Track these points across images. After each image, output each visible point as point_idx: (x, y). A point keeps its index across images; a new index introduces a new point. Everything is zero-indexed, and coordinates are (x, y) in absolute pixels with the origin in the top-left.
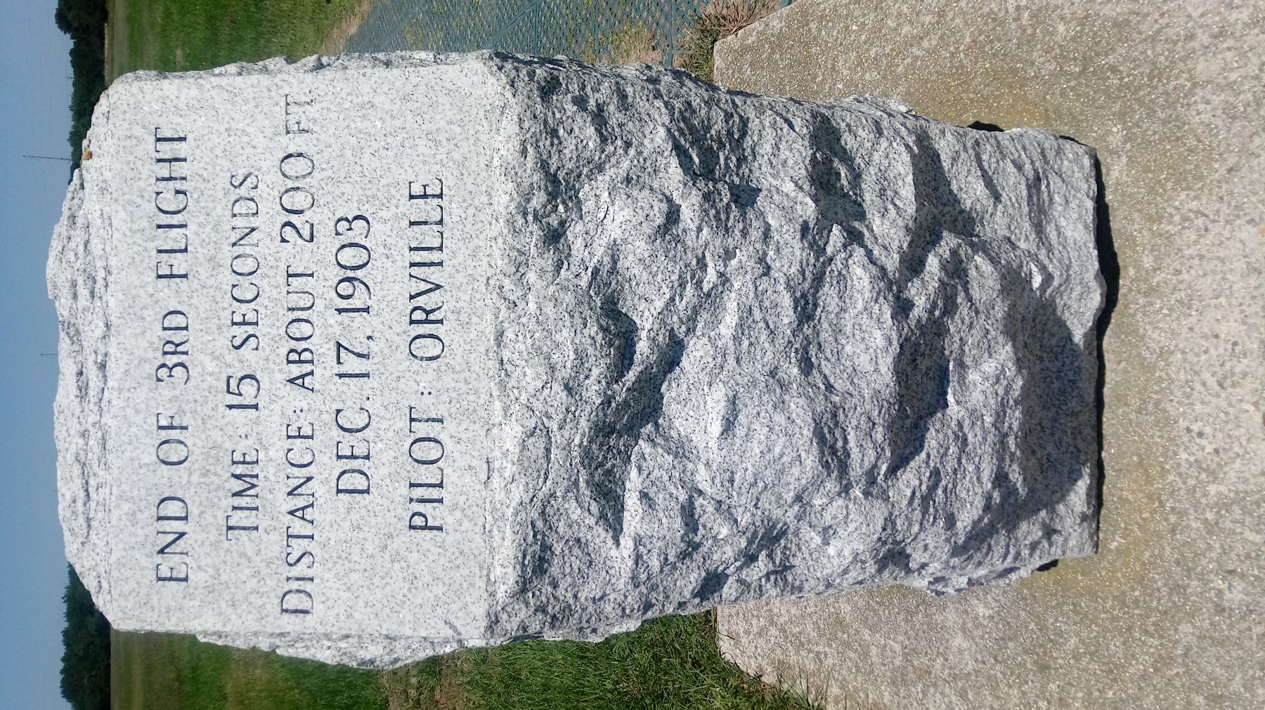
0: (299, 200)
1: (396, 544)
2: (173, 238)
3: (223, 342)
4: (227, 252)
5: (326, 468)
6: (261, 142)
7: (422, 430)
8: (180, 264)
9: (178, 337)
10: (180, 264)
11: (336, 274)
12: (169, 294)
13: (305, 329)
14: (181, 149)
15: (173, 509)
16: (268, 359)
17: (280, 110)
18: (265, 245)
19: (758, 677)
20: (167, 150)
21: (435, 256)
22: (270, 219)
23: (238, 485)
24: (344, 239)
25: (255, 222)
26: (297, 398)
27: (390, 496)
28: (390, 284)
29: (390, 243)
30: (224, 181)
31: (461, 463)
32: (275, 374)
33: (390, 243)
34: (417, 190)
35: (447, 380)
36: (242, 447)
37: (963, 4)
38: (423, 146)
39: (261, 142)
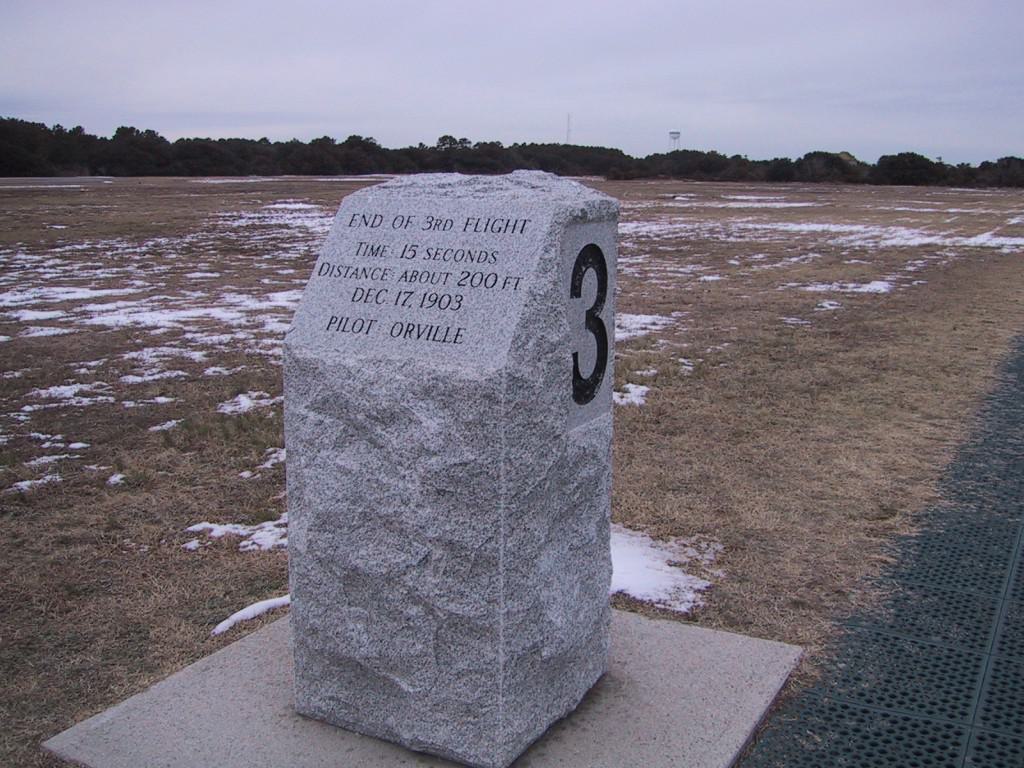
0: (476, 281)
5: (366, 283)
6: (506, 266)
7: (366, 325)
8: (470, 229)
9: (441, 226)
14: (517, 232)
16: (419, 264)
17: (517, 274)
21: (431, 337)
23: (375, 248)
25: (475, 262)
28: (427, 317)
34: (461, 332)
35: (381, 337)
39: (506, 266)
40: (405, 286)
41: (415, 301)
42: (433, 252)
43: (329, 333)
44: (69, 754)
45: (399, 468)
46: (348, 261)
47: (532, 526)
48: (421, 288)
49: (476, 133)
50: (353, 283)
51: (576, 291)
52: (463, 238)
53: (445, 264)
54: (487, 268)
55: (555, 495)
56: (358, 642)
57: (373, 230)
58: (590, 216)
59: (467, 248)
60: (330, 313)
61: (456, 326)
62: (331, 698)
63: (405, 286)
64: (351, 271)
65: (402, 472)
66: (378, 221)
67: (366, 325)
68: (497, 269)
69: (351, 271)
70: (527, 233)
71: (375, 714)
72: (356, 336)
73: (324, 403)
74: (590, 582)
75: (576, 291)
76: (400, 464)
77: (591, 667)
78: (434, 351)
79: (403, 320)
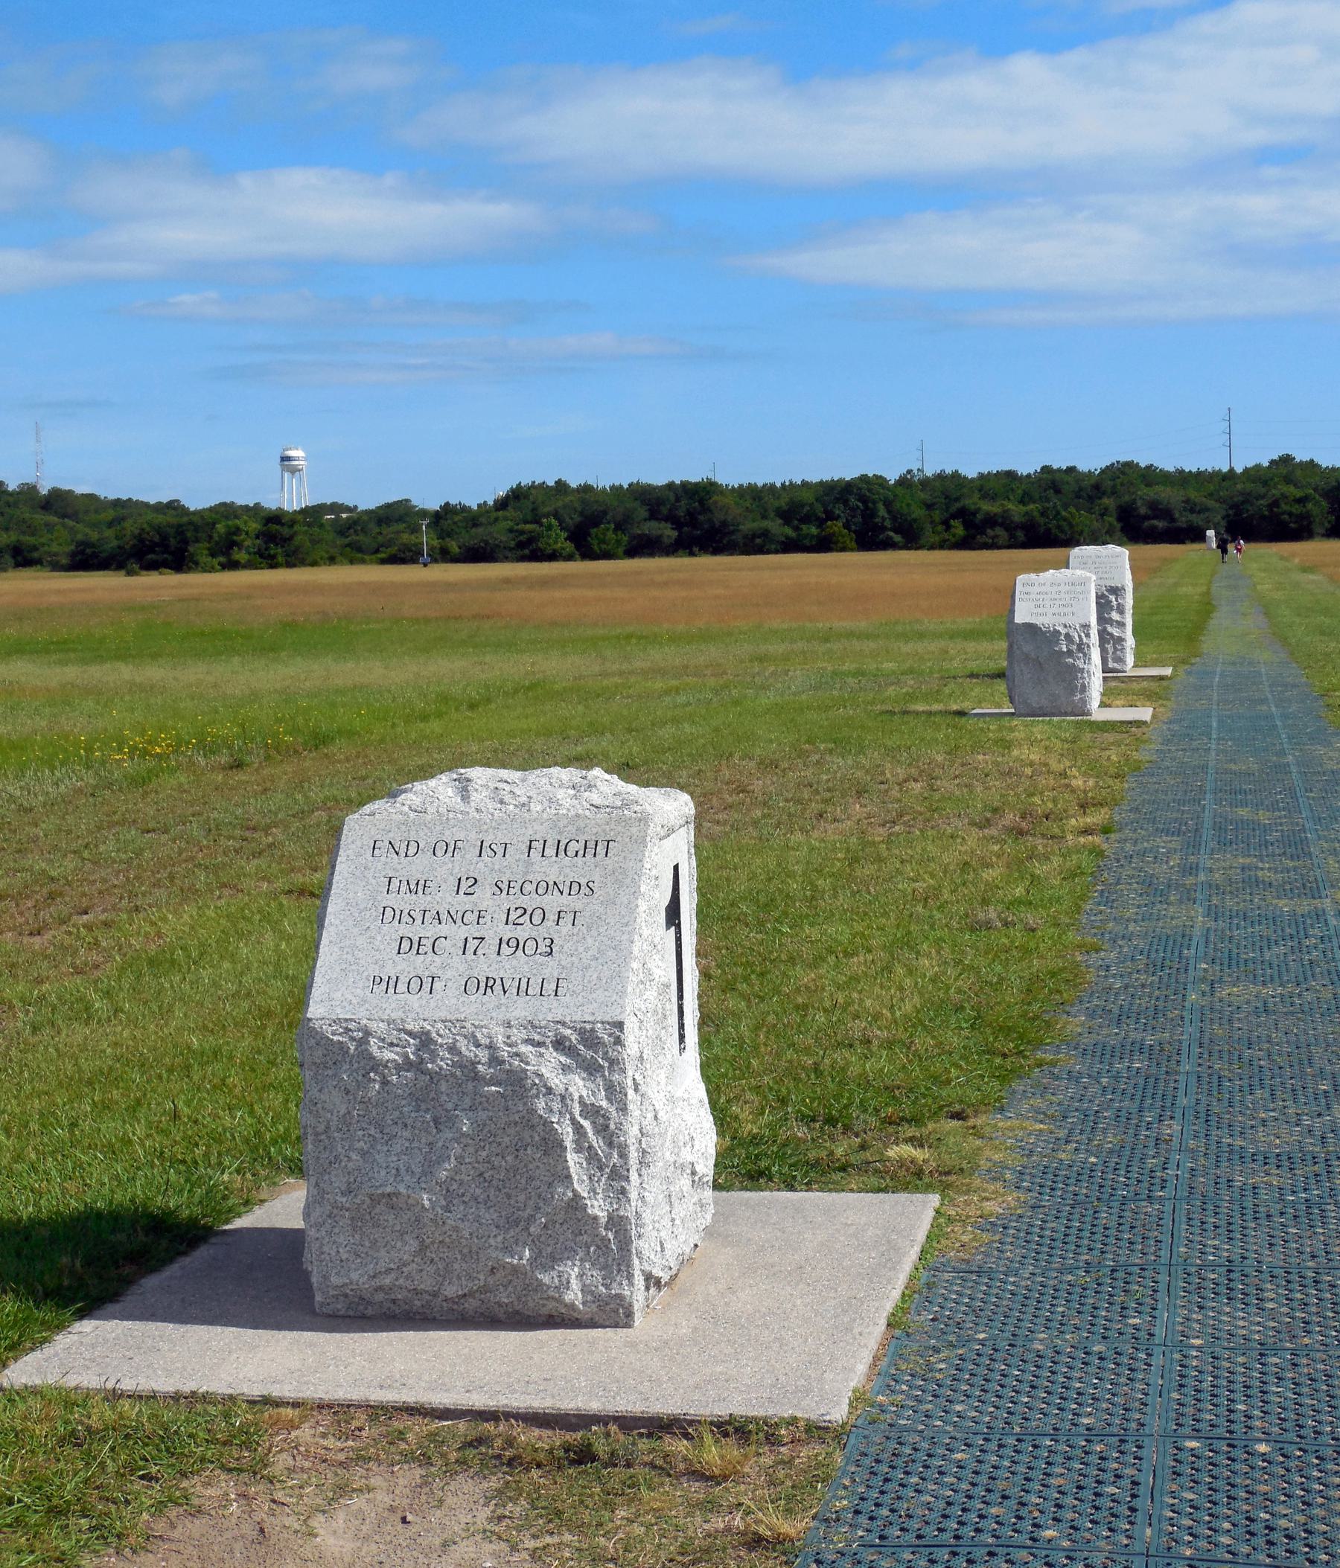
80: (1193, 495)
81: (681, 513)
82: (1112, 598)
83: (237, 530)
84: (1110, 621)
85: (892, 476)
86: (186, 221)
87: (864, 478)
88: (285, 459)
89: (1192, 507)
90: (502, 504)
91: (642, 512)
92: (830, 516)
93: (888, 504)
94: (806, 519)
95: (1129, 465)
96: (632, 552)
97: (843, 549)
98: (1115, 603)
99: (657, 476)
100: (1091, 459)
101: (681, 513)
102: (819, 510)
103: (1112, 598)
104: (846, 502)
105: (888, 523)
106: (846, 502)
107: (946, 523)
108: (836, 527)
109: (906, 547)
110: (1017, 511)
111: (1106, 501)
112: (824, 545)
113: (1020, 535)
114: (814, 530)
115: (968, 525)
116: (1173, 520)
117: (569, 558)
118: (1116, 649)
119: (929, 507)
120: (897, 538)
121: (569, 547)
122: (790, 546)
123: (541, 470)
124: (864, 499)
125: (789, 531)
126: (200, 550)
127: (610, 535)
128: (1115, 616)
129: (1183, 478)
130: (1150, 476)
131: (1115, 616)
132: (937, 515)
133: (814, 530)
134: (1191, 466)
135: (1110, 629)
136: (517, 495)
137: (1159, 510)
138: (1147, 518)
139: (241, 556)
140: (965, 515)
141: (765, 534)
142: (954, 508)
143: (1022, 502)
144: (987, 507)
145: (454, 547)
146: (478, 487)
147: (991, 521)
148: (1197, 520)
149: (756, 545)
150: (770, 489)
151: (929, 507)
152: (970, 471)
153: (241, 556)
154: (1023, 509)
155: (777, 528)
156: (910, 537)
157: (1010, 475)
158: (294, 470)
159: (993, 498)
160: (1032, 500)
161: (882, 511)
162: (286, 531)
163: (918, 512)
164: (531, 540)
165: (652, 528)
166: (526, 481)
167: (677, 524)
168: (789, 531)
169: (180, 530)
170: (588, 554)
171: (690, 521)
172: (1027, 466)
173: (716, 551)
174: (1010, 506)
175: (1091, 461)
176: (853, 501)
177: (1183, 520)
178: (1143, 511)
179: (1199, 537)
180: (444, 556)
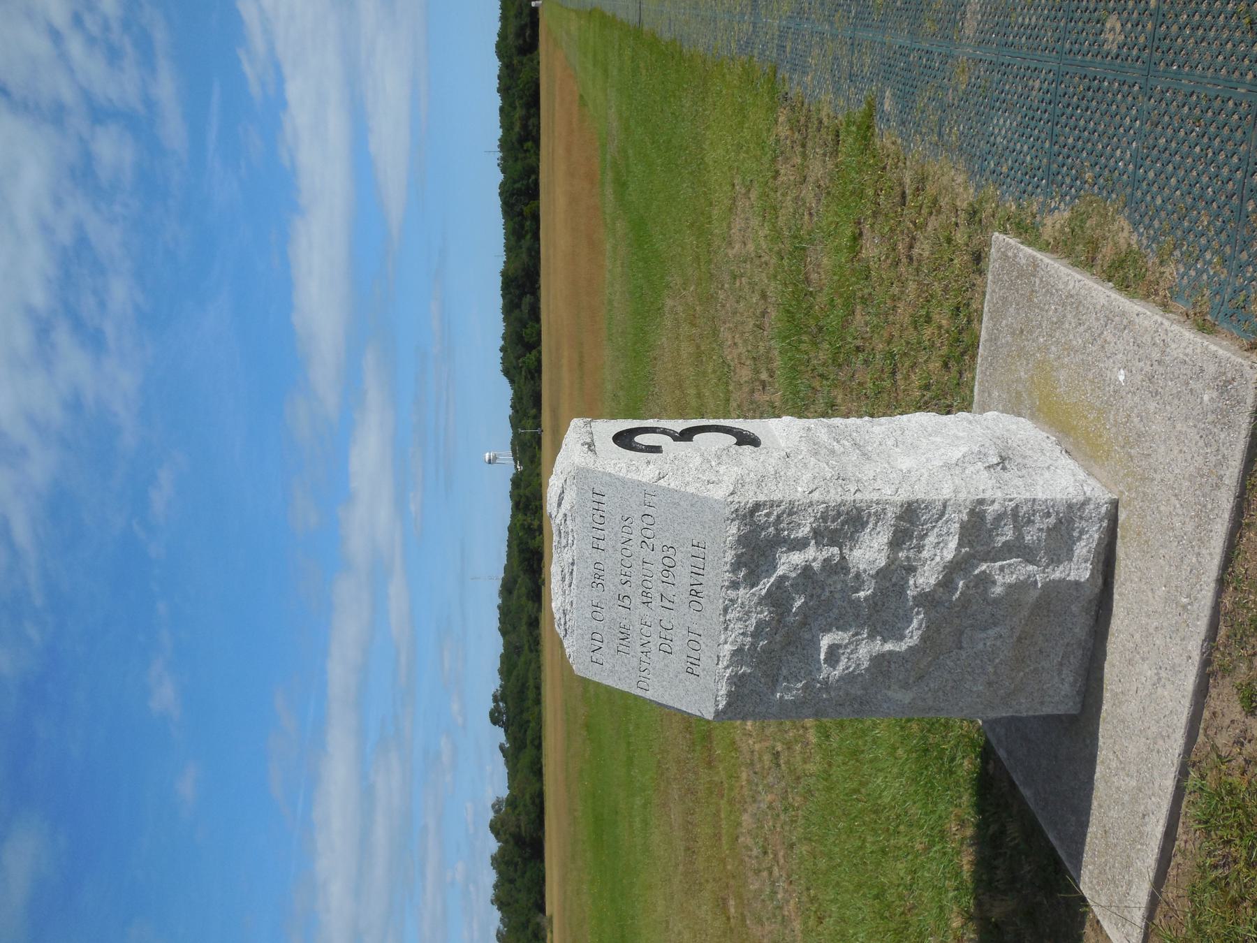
0: (649, 533)
1: (681, 676)
2: (599, 534)
3: (617, 580)
4: (619, 546)
5: (655, 641)
6: (635, 507)
7: (693, 637)
8: (602, 544)
9: (601, 573)
10: (602, 544)
11: (661, 567)
12: (597, 556)
13: (650, 585)
14: (604, 499)
15: (597, 637)
16: (634, 591)
17: (642, 495)
18: (634, 546)
19: (614, 16)
20: (597, 498)
21: (701, 572)
22: (636, 538)
23: (622, 636)
24: (665, 554)
25: (631, 537)
26: (643, 610)
27: (677, 662)
28: (683, 576)
29: (682, 557)
30: (619, 517)
31: (708, 654)
32: (637, 600)
33: (682, 557)
34: (695, 543)
35: (703, 621)
36: (624, 622)
37: (898, 4)
38: (698, 527)
39: (635, 507)
40: (656, 602)
41: (670, 592)
42: (624, 579)
43: (702, 674)
44: (888, 491)
45: (823, 598)
46: (635, 662)
47: (871, 474)
48: (656, 588)
49: (485, 680)
50: (656, 656)
51: (656, 449)
52: (611, 551)
53: (635, 566)
54: (637, 524)
55: (844, 459)
56: (996, 639)
57: (606, 641)
58: (589, 440)
59: (619, 546)
60: (684, 676)
61: (690, 548)
62: (1060, 673)
63: (656, 602)
64: (644, 658)
65: (827, 594)
66: (597, 637)
67: (693, 637)
68: (637, 515)
69: (644, 658)
70: (604, 490)
71: (1070, 625)
72: (703, 646)
73: (768, 676)
74: (930, 429)
75: (656, 449)
76: (819, 596)
77: (1014, 427)
78: (713, 568)
79: (687, 601)
80: (512, 13)
81: (517, 292)
82: (789, 562)
83: (522, 525)
84: (893, 577)
85: (501, 177)
86: (371, 514)
87: (501, 194)
88: (490, 462)
89: (519, 15)
90: (512, 381)
91: (517, 312)
92: (521, 214)
93: (515, 182)
94: (522, 226)
95: (498, 46)
96: (538, 320)
97: (538, 207)
98: (812, 555)
99: (499, 302)
100: (493, 66)
101: (517, 292)
102: (517, 219)
103: (789, 562)
104: (513, 205)
105: (525, 182)
106: (513, 205)
107: (527, 151)
108: (526, 210)
109: (537, 174)
110: (519, 113)
111: (515, 62)
112: (536, 218)
113: (532, 111)
114: (528, 223)
115: (527, 140)
116: (526, 25)
117: (540, 352)
118: (1018, 549)
119: (516, 159)
120: (533, 177)
121: (534, 352)
122: (536, 237)
123: (495, 359)
124: (512, 195)
125: (528, 237)
126: (533, 544)
127: (528, 331)
128: (869, 552)
129: (504, 18)
130: (503, 36)
131: (869, 552)
132: (521, 155)
133: (528, 223)
134: (498, 12)
135: (926, 578)
136: (506, 372)
137: (520, 33)
138: (525, 41)
139: (536, 523)
140: (522, 141)
141: (529, 250)
142: (516, 145)
143: (515, 108)
144: (517, 129)
145: (533, 411)
146: (503, 392)
147: (525, 127)
148: (526, 11)
149: (535, 254)
150: (506, 245)
151: (516, 159)
152: (499, 133)
153: (536, 523)
154: (518, 109)
155: (527, 241)
156: (533, 171)
157: (502, 110)
158: (495, 458)
159: (512, 123)
160: (514, 102)
161: (517, 185)
162: (523, 500)
163: (519, 166)
164: (530, 372)
165: (525, 307)
166: (500, 367)
167: (523, 294)
168: (528, 237)
169: (521, 551)
170: (538, 342)
171: (521, 287)
172: (497, 101)
173: (538, 274)
174: (517, 116)
175: (494, 65)
176: (513, 201)
177: (526, 19)
178: (521, 42)
179: (536, 10)
180: (538, 417)
